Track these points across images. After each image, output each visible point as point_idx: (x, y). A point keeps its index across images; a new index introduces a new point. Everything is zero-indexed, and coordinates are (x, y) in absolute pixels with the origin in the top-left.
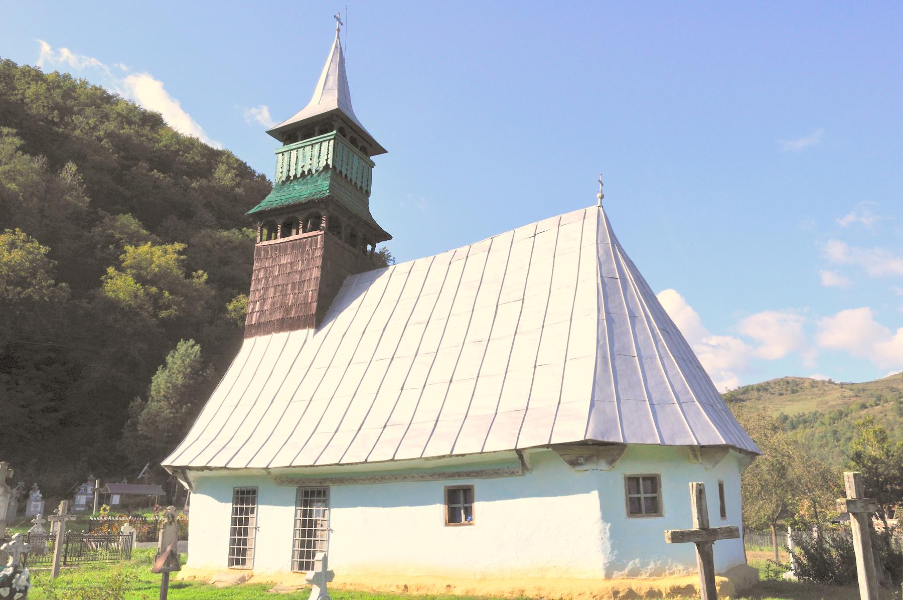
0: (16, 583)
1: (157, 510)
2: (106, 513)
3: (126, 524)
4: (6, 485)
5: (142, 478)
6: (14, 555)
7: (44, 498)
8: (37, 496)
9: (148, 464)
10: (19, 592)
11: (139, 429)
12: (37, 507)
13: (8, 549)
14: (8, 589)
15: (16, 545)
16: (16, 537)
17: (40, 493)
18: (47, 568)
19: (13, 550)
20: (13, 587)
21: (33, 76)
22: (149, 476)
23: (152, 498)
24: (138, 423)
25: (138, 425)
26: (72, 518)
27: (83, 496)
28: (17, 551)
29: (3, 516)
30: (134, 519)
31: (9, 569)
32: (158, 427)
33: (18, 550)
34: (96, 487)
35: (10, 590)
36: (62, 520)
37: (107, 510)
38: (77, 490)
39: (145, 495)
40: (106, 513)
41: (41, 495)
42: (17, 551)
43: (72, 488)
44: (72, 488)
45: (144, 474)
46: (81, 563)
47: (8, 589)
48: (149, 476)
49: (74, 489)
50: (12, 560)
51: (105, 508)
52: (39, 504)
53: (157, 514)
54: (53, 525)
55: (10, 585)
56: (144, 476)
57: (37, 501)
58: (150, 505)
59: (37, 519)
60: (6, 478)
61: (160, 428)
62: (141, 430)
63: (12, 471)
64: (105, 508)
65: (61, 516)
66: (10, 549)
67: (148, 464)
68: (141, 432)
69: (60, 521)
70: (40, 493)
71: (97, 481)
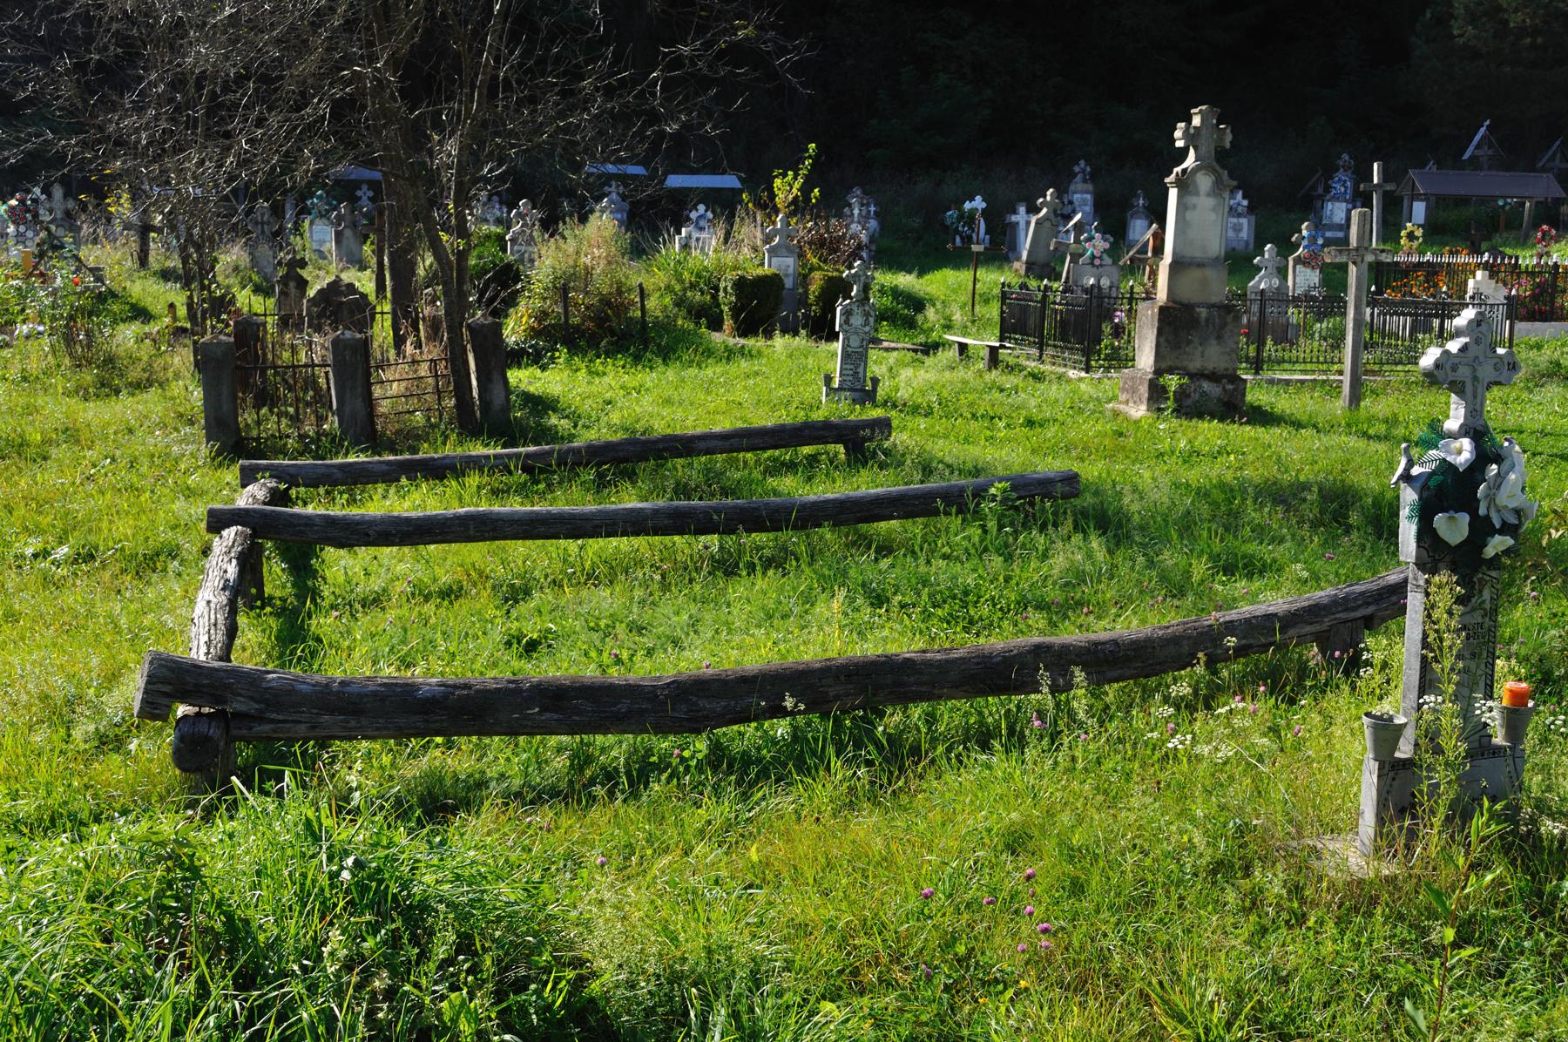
0: (1491, 499)
1: (1543, 239)
2: (1416, 244)
3: (1479, 274)
4: (1218, 168)
5: (1473, 158)
6: (1469, 389)
7: (1251, 209)
8: (1239, 204)
9: (1488, 122)
10: (1501, 532)
11: (1455, 32)
12: (1240, 230)
13: (1448, 367)
14: (1464, 519)
15: (1473, 351)
16: (1470, 322)
17: (1244, 198)
18: (1312, 377)
19: (1464, 373)
20: (1482, 511)
21: (852, 222)
22: (1490, 152)
23: (1507, 208)
24: (1452, 16)
25: (1453, 22)
26: (1384, 255)
27: (1337, 204)
28: (1475, 379)
29: (1217, 248)
30: (1495, 260)
31: (1456, 444)
32: (1506, 22)
33: (1480, 374)
34: (1376, 181)
35: (1470, 525)
36: (1359, 259)
37: (1417, 238)
38: (1320, 191)
39: (1484, 200)
40: (1416, 244)
41: (1245, 203)
42: (1475, 379)
43: (1310, 183)
44: (1310, 183)
45: (1478, 147)
46: (1385, 368)
47: (1464, 519)
48: (1490, 152)
49: (1314, 188)
50: (1462, 411)
51: (1412, 232)
52: (1244, 221)
53: (1546, 250)
54: (1294, 271)
55: (1470, 505)
56: (1479, 152)
57: (1239, 215)
58: (1502, 224)
59: (1266, 256)
60: (1217, 152)
61: (1512, 25)
62: (1461, 36)
63: (1228, 131)
64: (1412, 232)
65: (1357, 249)
66: (1454, 368)
67: (1488, 122)
68: (1461, 41)
69: (1354, 263)
70: (1244, 198)
71: (1375, 165)
